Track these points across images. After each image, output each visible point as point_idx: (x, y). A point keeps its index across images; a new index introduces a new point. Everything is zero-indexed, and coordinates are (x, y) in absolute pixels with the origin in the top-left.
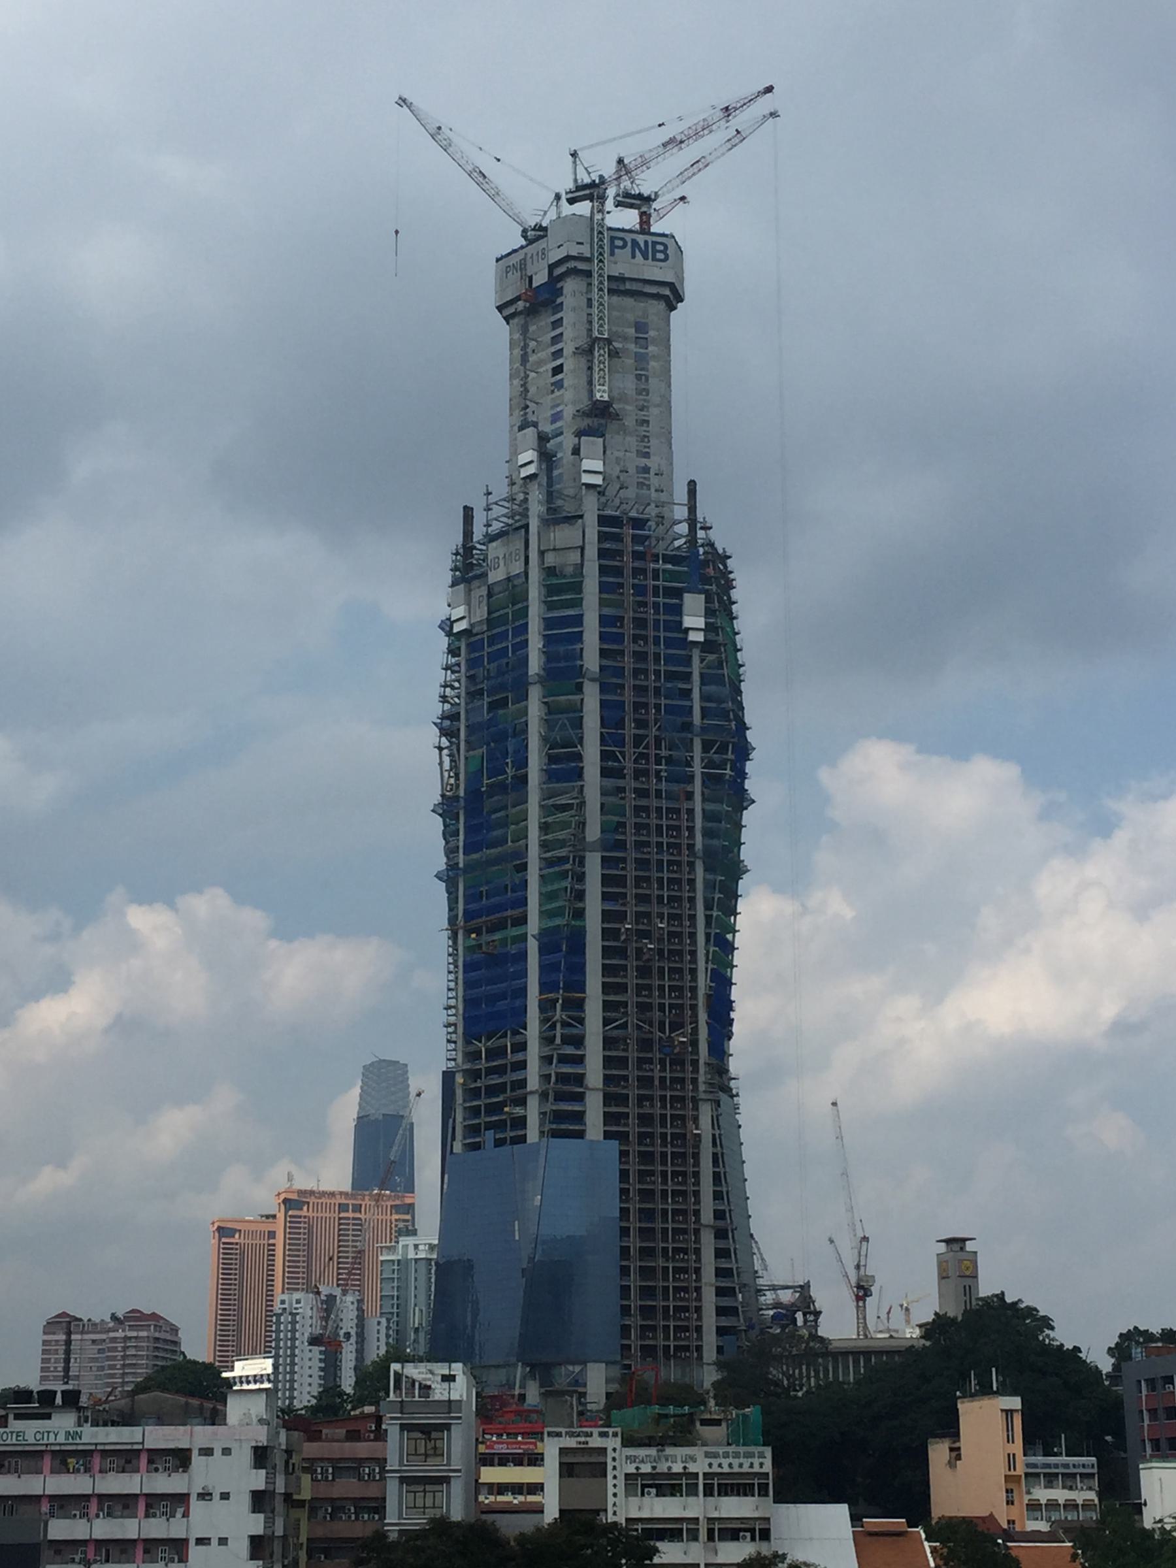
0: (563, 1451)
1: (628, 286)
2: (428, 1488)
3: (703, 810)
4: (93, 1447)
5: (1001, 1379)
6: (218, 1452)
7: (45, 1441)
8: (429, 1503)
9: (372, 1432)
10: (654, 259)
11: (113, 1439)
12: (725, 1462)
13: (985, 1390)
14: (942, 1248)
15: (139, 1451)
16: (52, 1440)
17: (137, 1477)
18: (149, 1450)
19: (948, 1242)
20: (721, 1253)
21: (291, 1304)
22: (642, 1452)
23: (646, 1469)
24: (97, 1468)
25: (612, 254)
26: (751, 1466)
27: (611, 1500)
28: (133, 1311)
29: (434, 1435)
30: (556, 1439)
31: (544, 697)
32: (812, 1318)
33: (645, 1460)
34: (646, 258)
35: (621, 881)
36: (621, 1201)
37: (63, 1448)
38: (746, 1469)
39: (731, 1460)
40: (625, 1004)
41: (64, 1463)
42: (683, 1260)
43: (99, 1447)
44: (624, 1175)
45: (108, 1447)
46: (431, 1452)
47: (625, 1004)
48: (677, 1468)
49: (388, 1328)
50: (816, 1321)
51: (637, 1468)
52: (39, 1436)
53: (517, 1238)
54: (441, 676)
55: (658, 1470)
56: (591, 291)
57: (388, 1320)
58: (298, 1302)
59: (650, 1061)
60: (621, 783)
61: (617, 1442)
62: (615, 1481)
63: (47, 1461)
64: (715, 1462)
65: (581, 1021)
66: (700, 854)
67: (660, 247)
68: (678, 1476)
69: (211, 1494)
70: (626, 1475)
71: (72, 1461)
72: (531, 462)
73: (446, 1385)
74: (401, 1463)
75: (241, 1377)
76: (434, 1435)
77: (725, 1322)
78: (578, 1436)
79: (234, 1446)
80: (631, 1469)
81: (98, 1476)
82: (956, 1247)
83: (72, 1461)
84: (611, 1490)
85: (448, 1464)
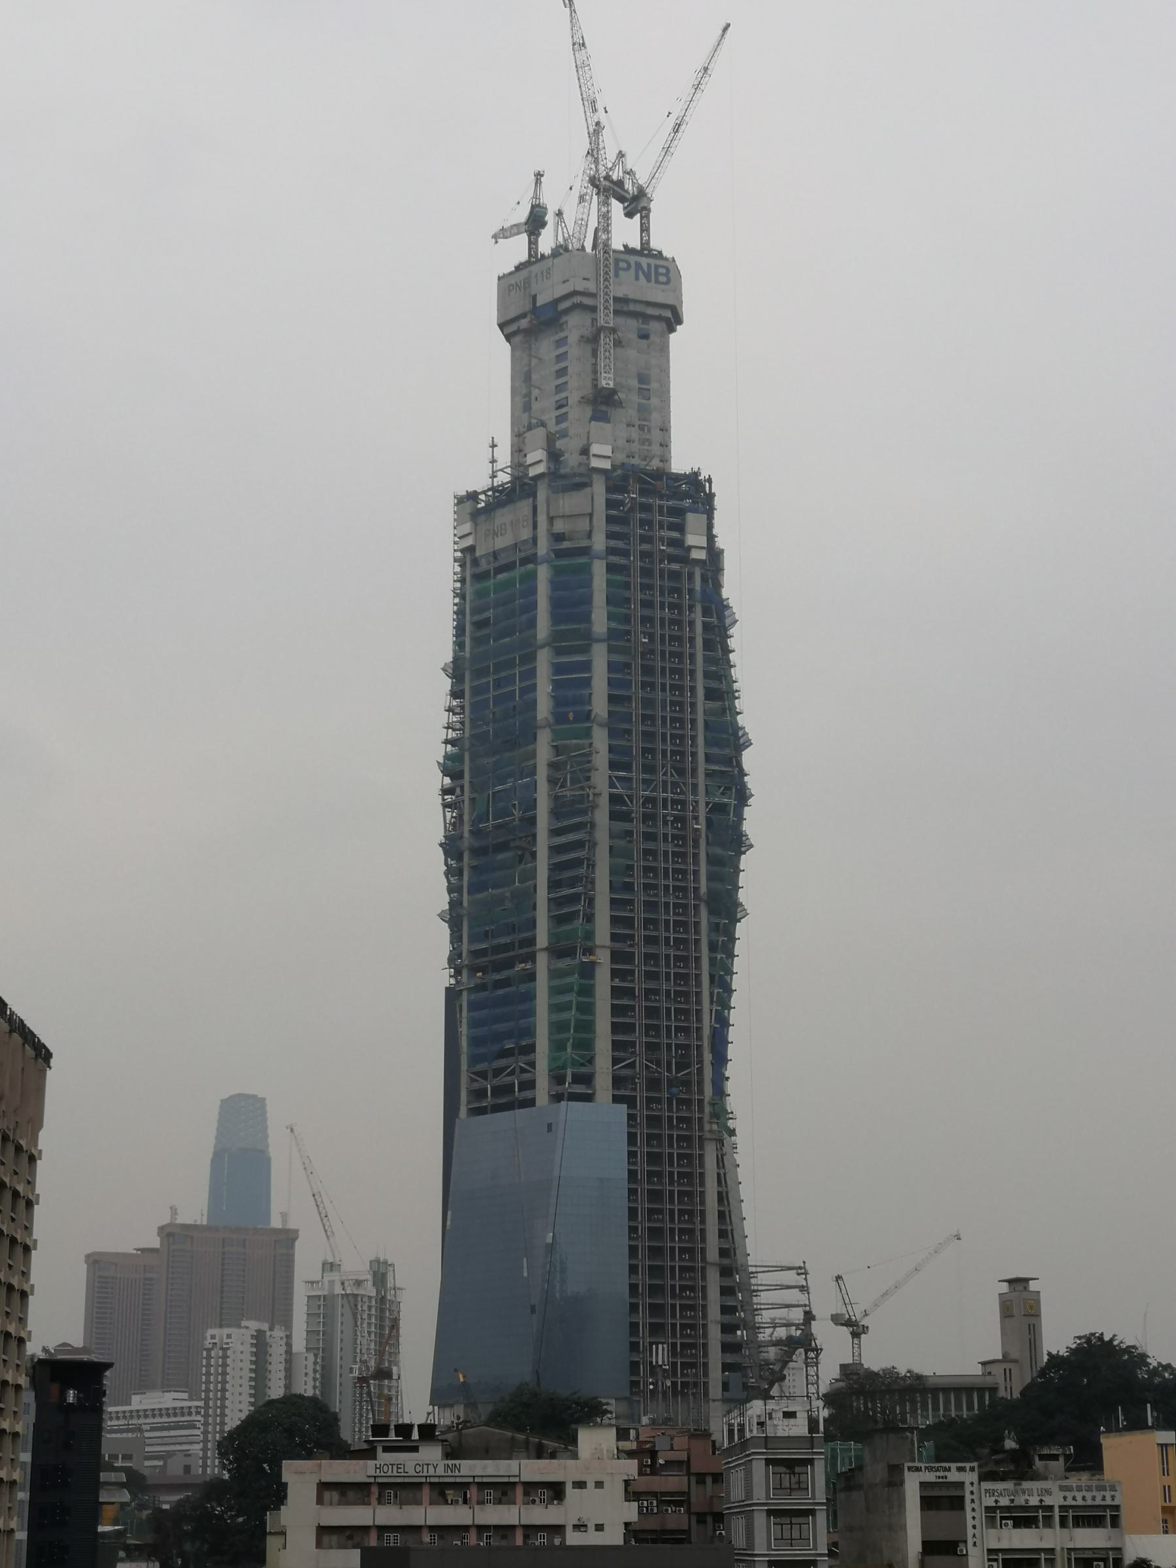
0: (923, 1485)
1: (632, 307)
2: (794, 1520)
3: (707, 854)
4: (471, 1480)
5: (1155, 1414)
6: (591, 1485)
7: (425, 1474)
8: (796, 1535)
9: (647, 1466)
10: (657, 282)
11: (490, 1471)
12: (1079, 1496)
13: (1137, 1424)
14: (1005, 1288)
15: (514, 1483)
16: (431, 1471)
17: (514, 1509)
18: (525, 1484)
19: (1011, 1282)
20: (726, 1291)
21: (221, 1340)
22: (999, 1486)
23: (1004, 1502)
24: (474, 1500)
25: (617, 275)
26: (1104, 1498)
27: (970, 1532)
28: (64, 1344)
29: (797, 1469)
30: (916, 1473)
31: (553, 741)
32: (812, 1355)
33: (1002, 1493)
34: (648, 280)
35: (628, 922)
36: (630, 1238)
37: (442, 1480)
38: (1098, 1502)
39: (1084, 1493)
40: (633, 1044)
41: (443, 1495)
42: (689, 1298)
43: (380, 1480)
44: (632, 1213)
45: (485, 1480)
46: (796, 1486)
47: (633, 1044)
48: (1034, 1501)
49: (315, 1363)
50: (817, 1357)
51: (996, 1501)
52: (419, 1469)
53: (525, 1274)
54: (444, 717)
55: (1016, 1503)
56: (589, 318)
57: (316, 1356)
58: (229, 1336)
59: (658, 1101)
60: (626, 826)
61: (974, 1477)
62: (974, 1514)
63: (426, 1490)
64: (1069, 1495)
65: (591, 1061)
66: (705, 898)
67: (664, 271)
68: (1036, 1508)
69: (586, 1526)
70: (986, 1508)
71: (450, 1493)
72: (541, 461)
73: (786, 1421)
74: (768, 1497)
75: (138, 1411)
76: (797, 1469)
77: (730, 1359)
78: (938, 1470)
79: (607, 1480)
80: (990, 1502)
81: (476, 1507)
82: (1020, 1287)
83: (450, 1493)
84: (970, 1522)
85: (814, 1497)
